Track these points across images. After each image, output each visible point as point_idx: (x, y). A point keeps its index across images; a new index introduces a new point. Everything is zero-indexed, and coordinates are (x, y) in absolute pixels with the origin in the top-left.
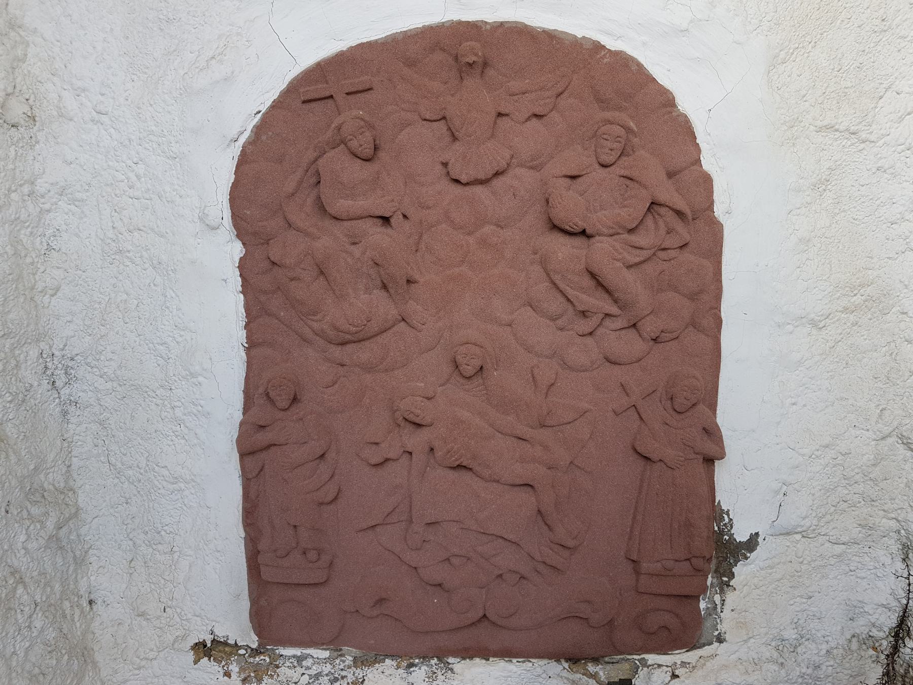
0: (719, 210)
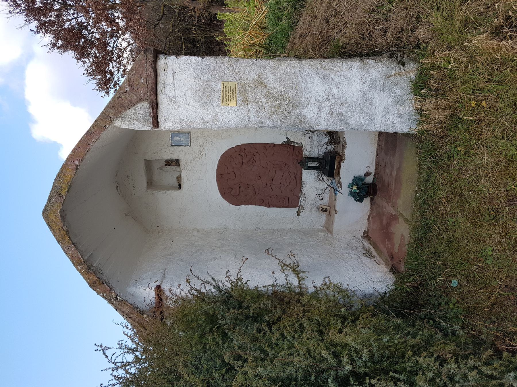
0: (240, 144)
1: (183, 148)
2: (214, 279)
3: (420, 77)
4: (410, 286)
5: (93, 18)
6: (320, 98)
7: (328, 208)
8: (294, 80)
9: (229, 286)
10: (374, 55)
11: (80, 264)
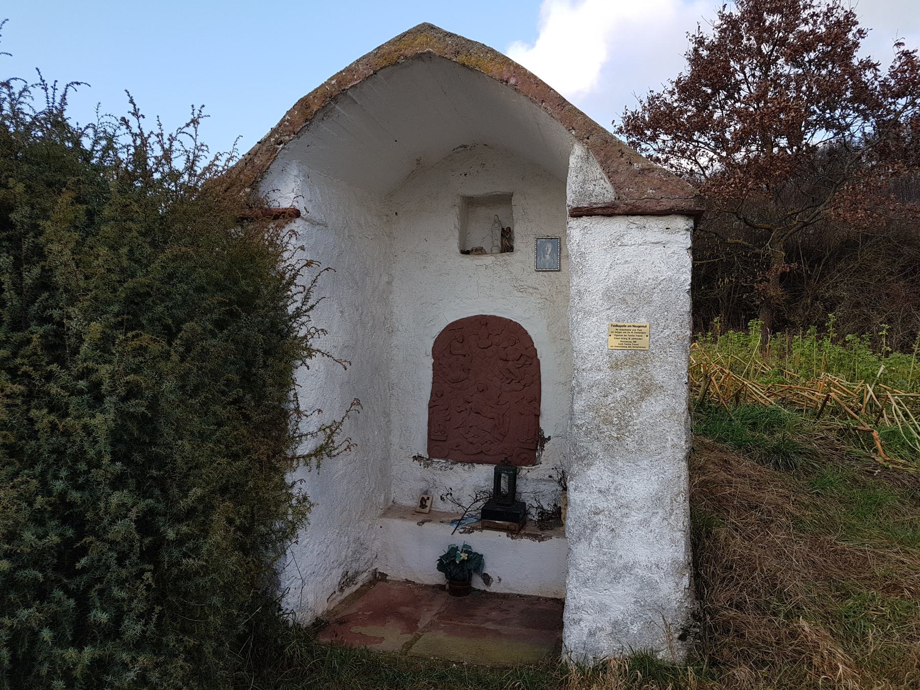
1: (533, 260)
2: (312, 307)
3: (660, 666)
4: (294, 652)
5: (747, 109)
6: (622, 493)
7: (427, 510)
8: (653, 447)
9: (302, 334)
10: (697, 586)
11: (339, 82)
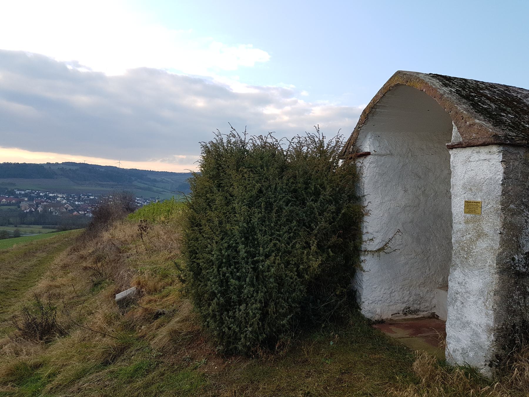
6: (467, 286)
8: (480, 265)
